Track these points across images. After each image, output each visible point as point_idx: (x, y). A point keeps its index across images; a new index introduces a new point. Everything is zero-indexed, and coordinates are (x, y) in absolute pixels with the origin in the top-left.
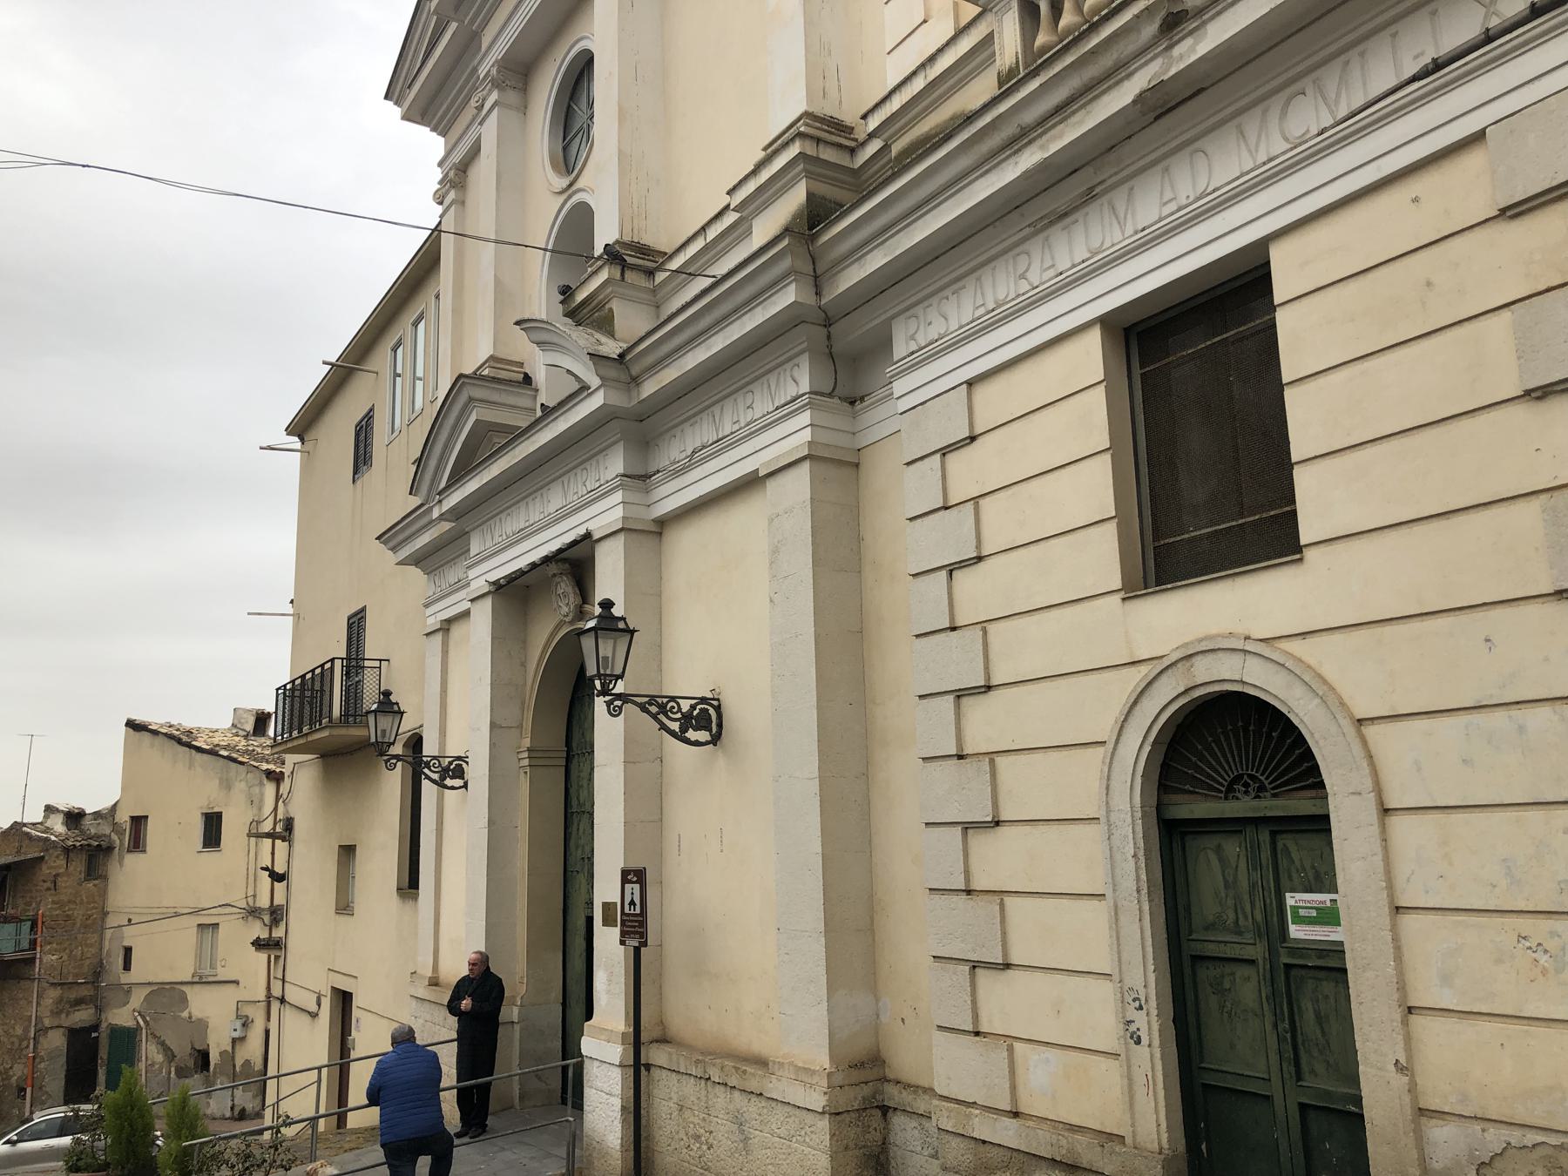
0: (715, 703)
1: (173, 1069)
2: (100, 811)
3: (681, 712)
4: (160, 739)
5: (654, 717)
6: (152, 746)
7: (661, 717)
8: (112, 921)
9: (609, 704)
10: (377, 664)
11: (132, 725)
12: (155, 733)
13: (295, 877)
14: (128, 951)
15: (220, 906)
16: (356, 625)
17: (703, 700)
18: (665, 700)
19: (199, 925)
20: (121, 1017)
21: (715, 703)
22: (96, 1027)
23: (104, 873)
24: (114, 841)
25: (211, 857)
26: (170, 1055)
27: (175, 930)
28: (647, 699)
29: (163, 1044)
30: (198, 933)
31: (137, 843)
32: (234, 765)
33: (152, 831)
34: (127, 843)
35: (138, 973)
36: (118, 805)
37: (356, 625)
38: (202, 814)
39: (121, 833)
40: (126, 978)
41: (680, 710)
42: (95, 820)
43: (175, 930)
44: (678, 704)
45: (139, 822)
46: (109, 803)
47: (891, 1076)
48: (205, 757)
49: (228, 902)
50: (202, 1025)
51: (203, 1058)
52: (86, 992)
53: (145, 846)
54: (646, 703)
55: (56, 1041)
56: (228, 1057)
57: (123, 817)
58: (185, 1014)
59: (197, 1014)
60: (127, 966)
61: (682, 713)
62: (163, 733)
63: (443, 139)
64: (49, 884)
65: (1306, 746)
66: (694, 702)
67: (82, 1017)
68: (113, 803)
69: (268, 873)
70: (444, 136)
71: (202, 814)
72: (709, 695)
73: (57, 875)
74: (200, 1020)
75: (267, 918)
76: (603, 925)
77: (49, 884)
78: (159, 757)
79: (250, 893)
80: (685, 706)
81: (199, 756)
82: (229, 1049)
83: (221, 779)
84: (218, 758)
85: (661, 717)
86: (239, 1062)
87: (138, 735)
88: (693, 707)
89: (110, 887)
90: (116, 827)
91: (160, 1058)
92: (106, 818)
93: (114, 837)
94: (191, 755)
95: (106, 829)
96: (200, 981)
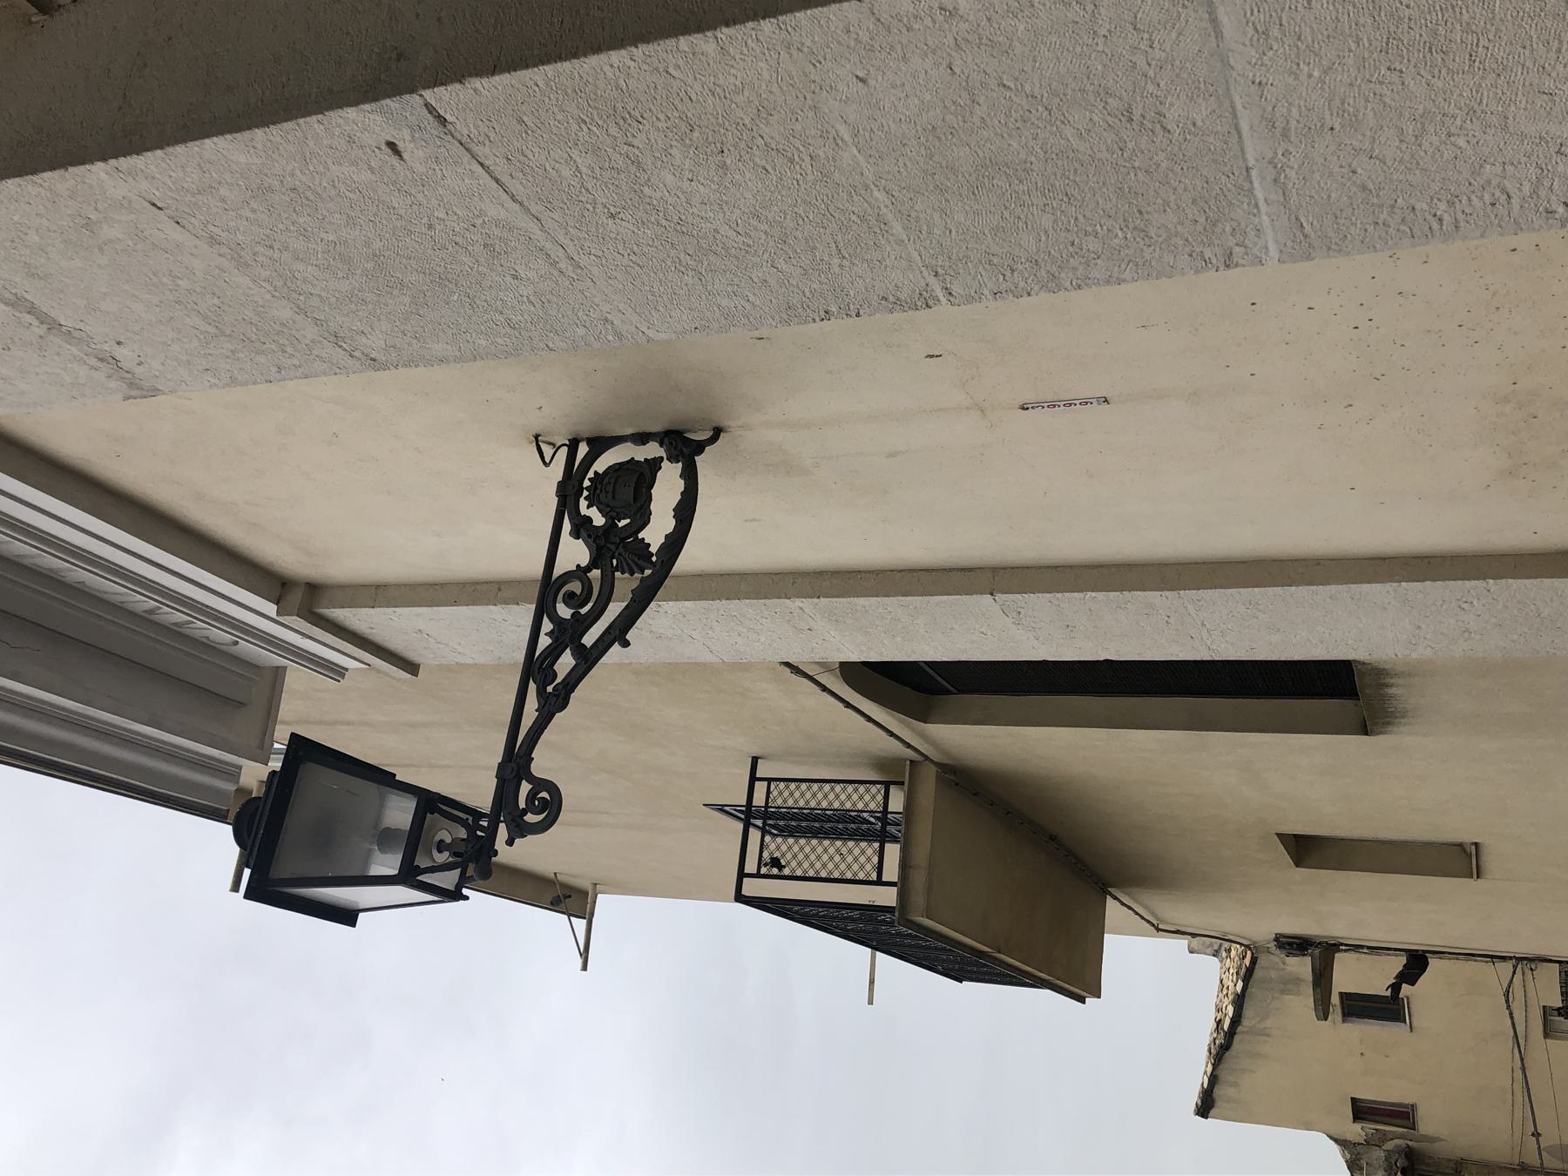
0: (583, 449)
2: (1346, 1162)
3: (588, 569)
4: (1223, 1074)
5: (588, 659)
6: (1235, 1085)
7: (589, 639)
8: (1532, 1159)
9: (520, 829)
11: (1205, 1107)
12: (1213, 1079)
13: (1417, 938)
15: (1508, 1007)
17: (567, 493)
18: (547, 626)
19: (1546, 1035)
21: (583, 449)
23: (1452, 1165)
24: (1396, 1146)
28: (532, 687)
30: (1556, 1038)
31: (1403, 1115)
32: (1258, 973)
33: (1374, 1092)
34: (1401, 1130)
36: (1332, 1133)
38: (1344, 1021)
39: (1381, 1139)
41: (581, 572)
42: (1362, 1169)
44: (568, 577)
45: (1361, 1110)
46: (1335, 1149)
47: (1042, 291)
48: (1248, 1012)
49: (1500, 993)
53: (1406, 1106)
54: (541, 692)
57: (1356, 1131)
61: (594, 564)
62: (1214, 1070)
63: (276, 607)
66: (567, 526)
68: (1328, 1139)
69: (1404, 985)
70: (277, 604)
71: (1344, 1021)
72: (557, 470)
78: (1250, 1078)
80: (574, 553)
81: (1246, 1023)
83: (1283, 992)
84: (1246, 994)
85: (589, 639)
87: (1219, 1103)
88: (582, 527)
89: (1476, 1157)
92: (1359, 1153)
93: (1390, 1145)
94: (1243, 1032)
95: (1378, 1155)
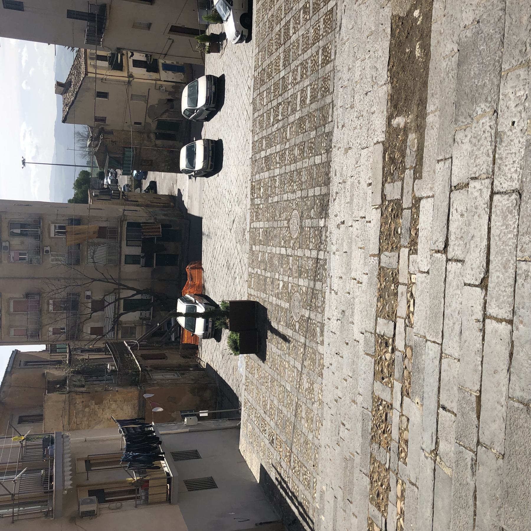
1: (171, 110)
10: (89, 5)
14: (136, 123)
16: (71, 14)
20: (154, 126)
22: (156, 133)
25: (110, 96)
26: (167, 111)
27: (101, 209)
29: (163, 113)
31: (103, 120)
35: (142, 121)
37: (71, 14)
40: (143, 124)
43: (101, 209)
45: (97, 119)
50: (160, 101)
51: (169, 100)
52: (145, 135)
55: (159, 142)
56: (170, 93)
58: (156, 106)
59: (156, 102)
60: (140, 124)
64: (114, 144)
65: (256, 303)
67: (152, 136)
73: (112, 141)
74: (159, 101)
75: (131, 79)
76: (67, 17)
77: (114, 144)
79: (123, 83)
82: (168, 93)
86: (172, 90)
90: (97, 126)
91: (167, 114)
93: (100, 127)
96: (147, 101)
